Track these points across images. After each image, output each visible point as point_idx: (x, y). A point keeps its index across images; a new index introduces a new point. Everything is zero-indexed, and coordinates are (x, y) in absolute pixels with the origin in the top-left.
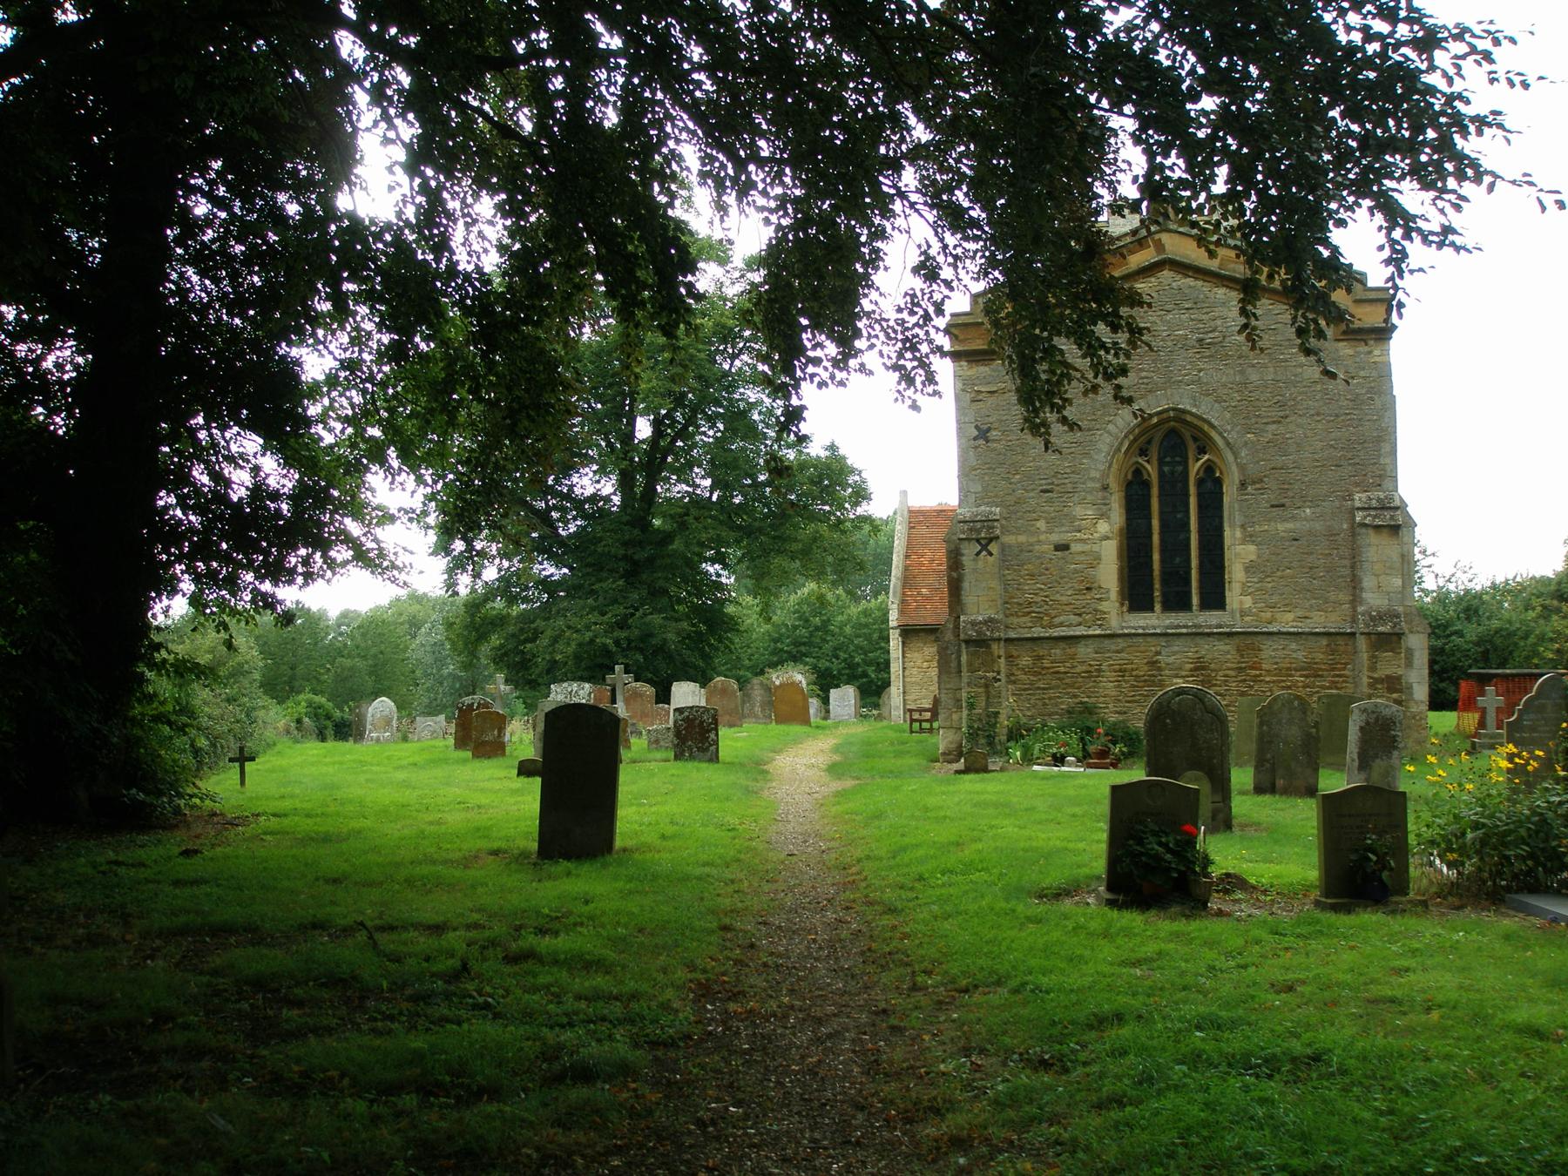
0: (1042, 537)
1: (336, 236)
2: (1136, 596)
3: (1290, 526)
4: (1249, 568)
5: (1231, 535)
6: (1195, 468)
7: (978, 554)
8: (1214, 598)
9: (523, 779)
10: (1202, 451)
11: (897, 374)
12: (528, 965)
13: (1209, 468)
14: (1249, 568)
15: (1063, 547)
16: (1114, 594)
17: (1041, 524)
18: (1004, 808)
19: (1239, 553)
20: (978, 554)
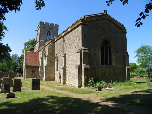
0: (92, 53)
1: (14, 6)
2: (103, 64)
3: (118, 54)
4: (115, 59)
5: (112, 55)
6: (109, 46)
7: (85, 54)
8: (110, 64)
9: (7, 99)
10: (109, 44)
11: (2, 39)
12: (134, 87)
13: (110, 46)
14: (115, 59)
15: (95, 55)
16: (101, 62)
17: (92, 51)
18: (129, 87)
19: (113, 58)
20: (85, 54)
